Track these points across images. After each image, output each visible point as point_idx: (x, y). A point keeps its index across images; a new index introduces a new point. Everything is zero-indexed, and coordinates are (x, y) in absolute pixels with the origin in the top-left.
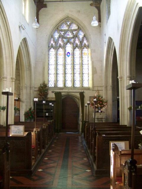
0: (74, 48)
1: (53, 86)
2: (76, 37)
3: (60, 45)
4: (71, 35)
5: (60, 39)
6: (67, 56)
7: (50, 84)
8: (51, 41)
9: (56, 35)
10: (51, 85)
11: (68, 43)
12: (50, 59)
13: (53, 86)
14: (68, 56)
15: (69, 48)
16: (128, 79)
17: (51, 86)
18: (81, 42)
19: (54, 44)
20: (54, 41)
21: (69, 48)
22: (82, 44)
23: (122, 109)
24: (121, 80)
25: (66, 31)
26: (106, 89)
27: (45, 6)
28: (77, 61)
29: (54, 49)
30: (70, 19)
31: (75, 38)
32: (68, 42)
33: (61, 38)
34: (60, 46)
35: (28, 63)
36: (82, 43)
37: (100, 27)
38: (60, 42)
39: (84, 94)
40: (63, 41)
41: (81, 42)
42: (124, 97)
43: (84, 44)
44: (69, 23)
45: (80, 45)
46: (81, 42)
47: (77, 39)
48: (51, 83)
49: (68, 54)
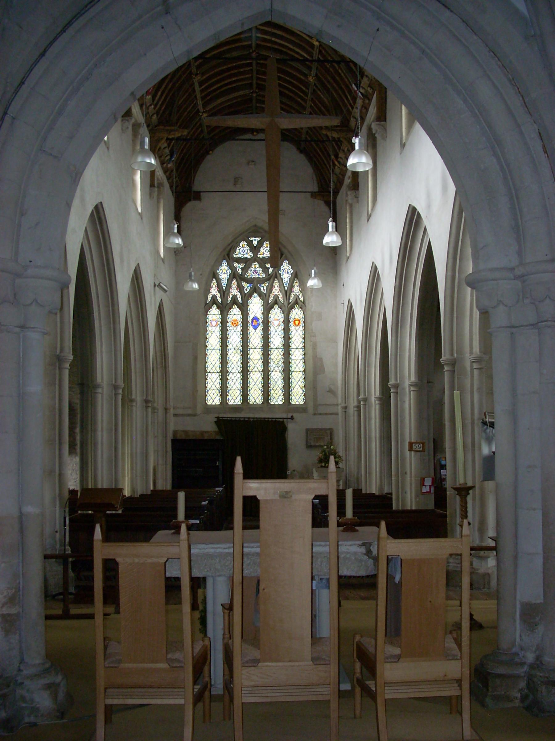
0: (267, 309)
1: (217, 402)
2: (276, 277)
3: (234, 297)
4: (261, 271)
5: (234, 284)
6: (251, 328)
7: (209, 398)
8: (211, 287)
9: (224, 272)
10: (211, 401)
11: (255, 294)
12: (210, 334)
13: (217, 402)
14: (255, 328)
15: (255, 307)
16: (377, 402)
17: (214, 404)
18: (286, 292)
19: (218, 295)
20: (219, 286)
21: (255, 307)
22: (290, 296)
23: (366, 461)
24: (366, 405)
25: (247, 263)
26: (346, 412)
27: (197, 196)
28: (276, 340)
29: (218, 308)
30: (261, 231)
31: (272, 280)
32: (255, 290)
33: (237, 280)
34: (234, 301)
35: (161, 352)
36: (290, 294)
37: (336, 255)
38: (234, 291)
39: (198, 202)
40: (240, 289)
41: (287, 293)
42: (370, 438)
43: (295, 295)
44: (258, 241)
45: (284, 301)
46: (287, 293)
47: (276, 284)
48: (212, 395)
49: (255, 322)
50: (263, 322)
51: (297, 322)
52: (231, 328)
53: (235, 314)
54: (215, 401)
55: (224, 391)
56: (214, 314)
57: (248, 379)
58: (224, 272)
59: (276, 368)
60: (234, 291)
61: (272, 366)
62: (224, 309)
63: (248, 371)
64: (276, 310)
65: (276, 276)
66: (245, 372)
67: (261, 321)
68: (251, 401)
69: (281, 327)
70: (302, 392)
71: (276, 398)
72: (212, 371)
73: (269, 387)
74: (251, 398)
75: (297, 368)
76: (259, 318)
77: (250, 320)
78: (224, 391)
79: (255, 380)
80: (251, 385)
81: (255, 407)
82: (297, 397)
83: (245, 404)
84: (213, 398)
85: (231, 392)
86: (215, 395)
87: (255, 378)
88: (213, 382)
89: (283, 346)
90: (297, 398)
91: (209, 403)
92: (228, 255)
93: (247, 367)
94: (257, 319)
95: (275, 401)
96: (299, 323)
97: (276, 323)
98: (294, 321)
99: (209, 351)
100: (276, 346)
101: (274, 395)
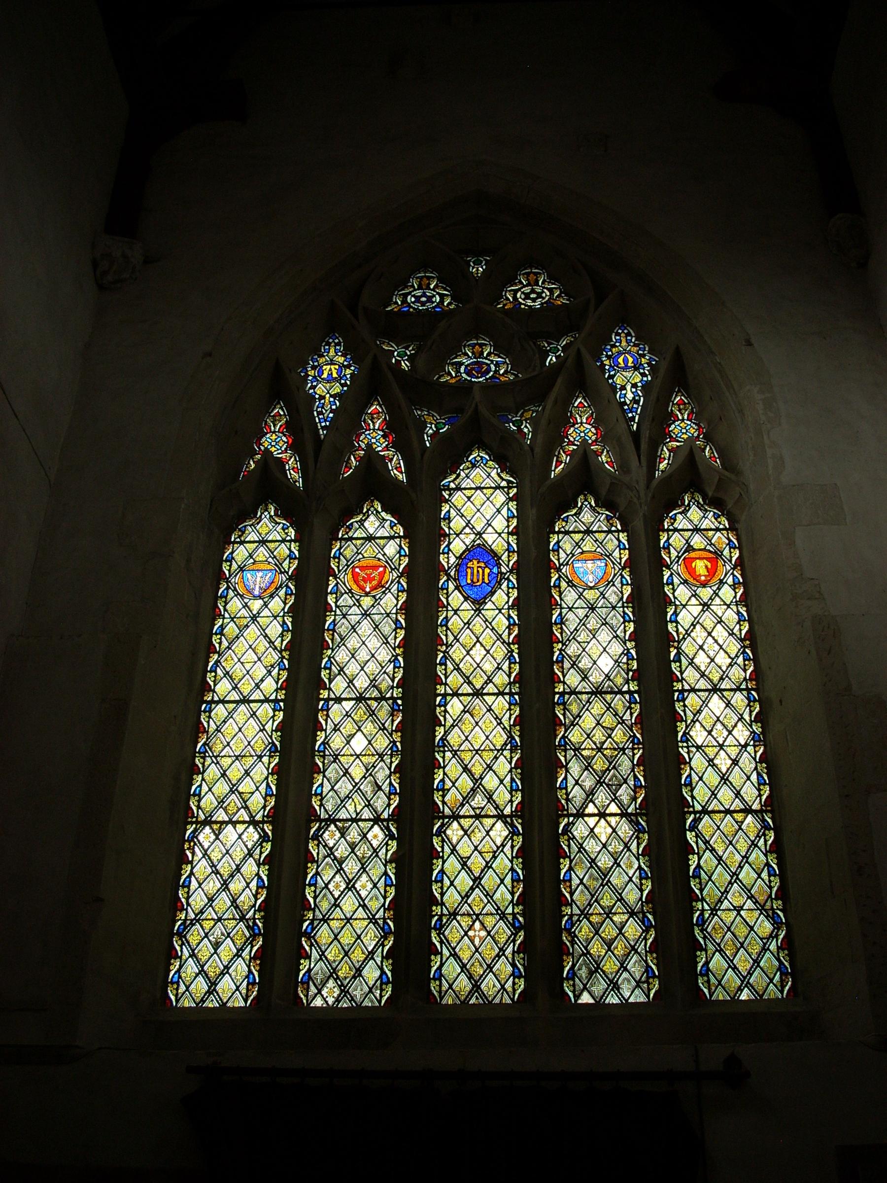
0: (539, 512)
9: (329, 377)
10: (200, 986)
12: (231, 629)
15: (480, 507)
21: (480, 507)
28: (598, 651)
33: (391, 407)
40: (401, 433)
50: (517, 569)
51: (701, 567)
52: (346, 600)
53: (376, 536)
54: (226, 985)
55: (283, 920)
56: (263, 550)
57: (435, 854)
58: (329, 377)
59: (602, 796)
60: (374, 436)
61: (575, 781)
62: (318, 519)
63: (434, 812)
64: (587, 516)
65: (584, 378)
66: (416, 820)
67: (509, 561)
68: (452, 979)
69: (620, 591)
70: (765, 927)
71: (610, 966)
72: (221, 816)
73: (561, 901)
74: (451, 968)
75: (725, 795)
76: (499, 546)
77: (448, 561)
78: (283, 920)
79: (476, 864)
80: (453, 884)
81: (476, 1020)
82: (743, 955)
83: (304, 955)
84: (214, 969)
85: (324, 934)
86: (227, 949)
87: (478, 854)
88: (224, 864)
89: (638, 676)
90: (743, 962)
91: (189, 986)
92: (360, 322)
93: (429, 791)
94: (492, 557)
95: (600, 986)
96: (712, 572)
97: (589, 571)
98: (688, 562)
99: (220, 711)
100: (596, 677)
101: (597, 948)
